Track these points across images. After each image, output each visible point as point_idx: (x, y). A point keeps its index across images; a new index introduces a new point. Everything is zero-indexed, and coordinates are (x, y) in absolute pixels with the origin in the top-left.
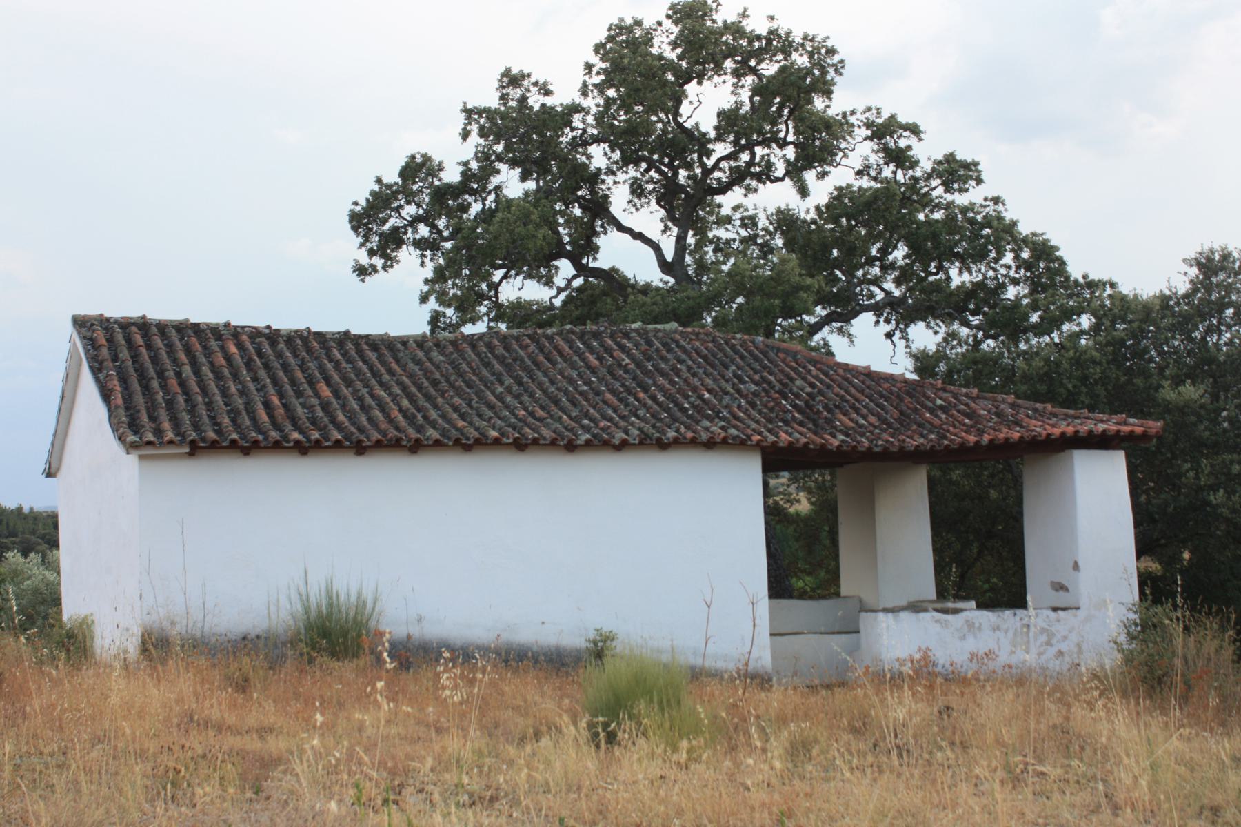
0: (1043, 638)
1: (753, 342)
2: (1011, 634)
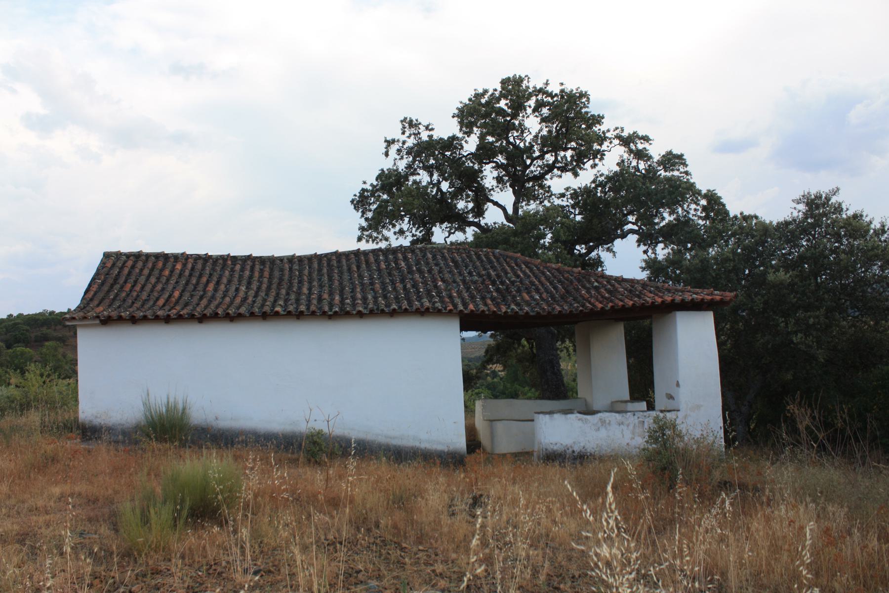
1: (493, 253)
2: (631, 427)
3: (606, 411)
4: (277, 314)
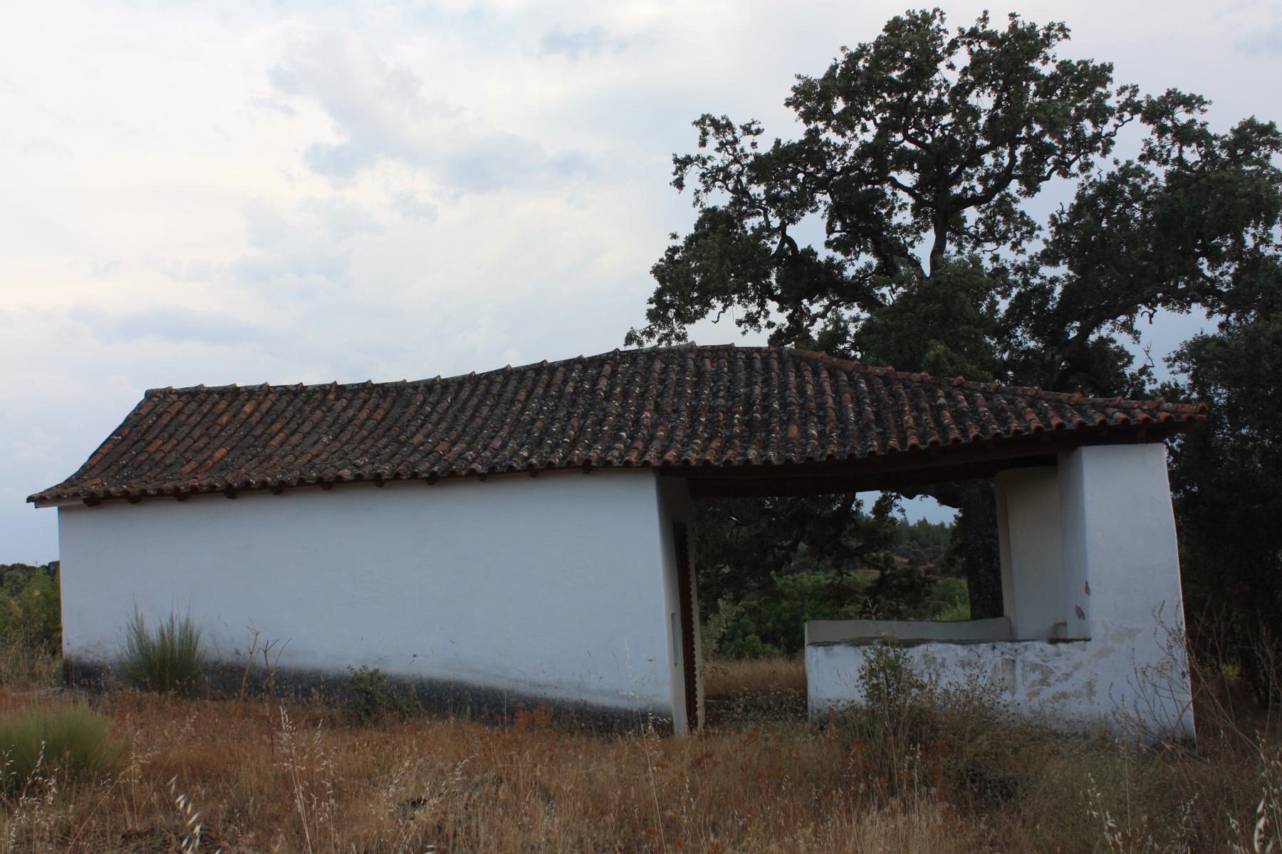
0: (1037, 676)
3: (939, 642)
4: (608, 465)
